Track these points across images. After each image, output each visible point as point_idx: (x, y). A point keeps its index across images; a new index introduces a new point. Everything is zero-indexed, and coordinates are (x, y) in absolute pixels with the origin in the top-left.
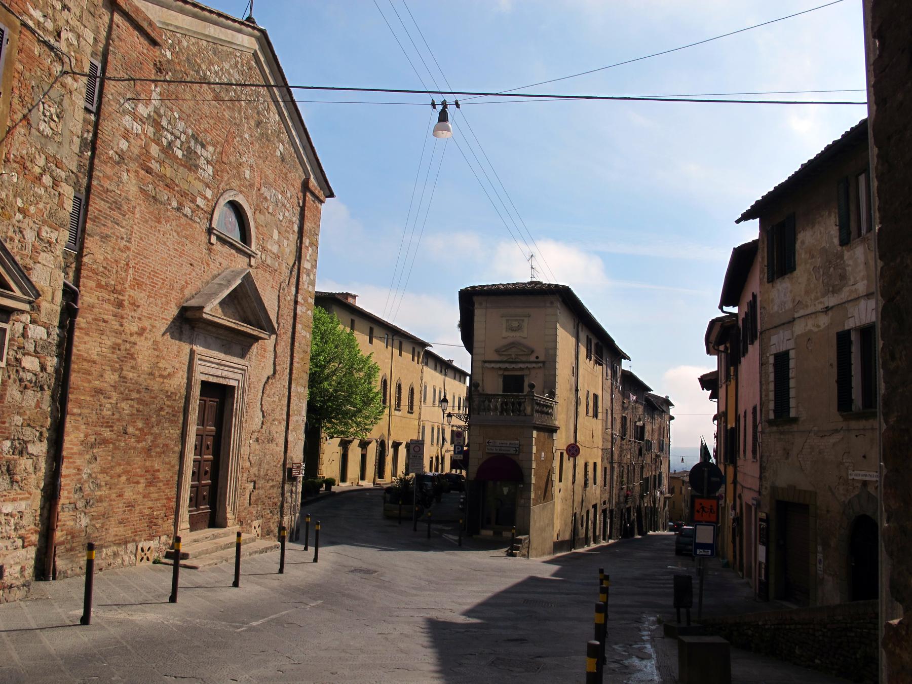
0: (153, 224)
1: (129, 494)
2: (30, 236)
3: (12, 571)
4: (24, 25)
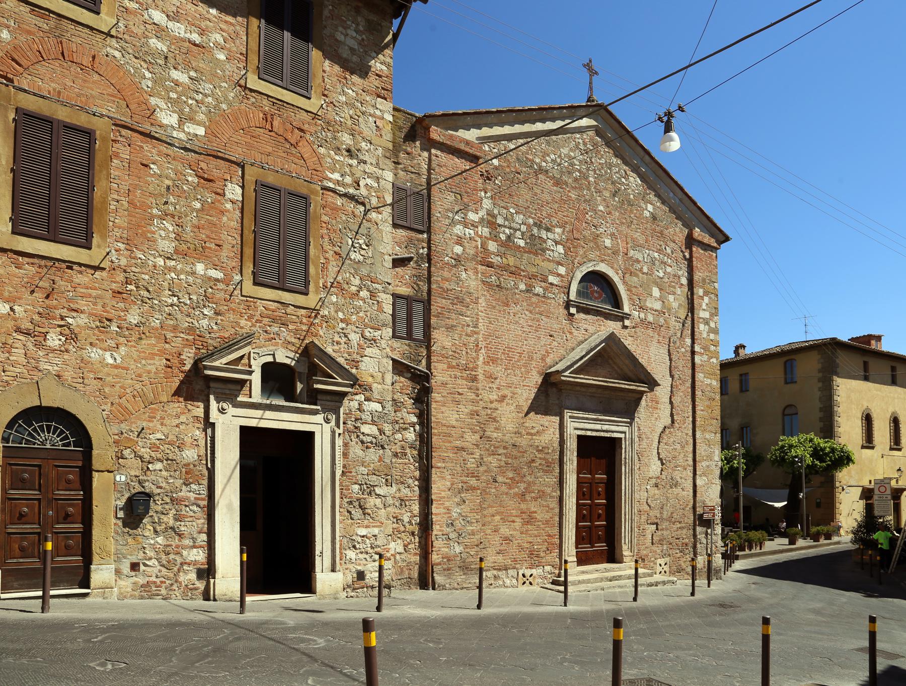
0: (502, 308)
1: (505, 531)
2: (354, 338)
3: (372, 576)
4: (325, 188)
